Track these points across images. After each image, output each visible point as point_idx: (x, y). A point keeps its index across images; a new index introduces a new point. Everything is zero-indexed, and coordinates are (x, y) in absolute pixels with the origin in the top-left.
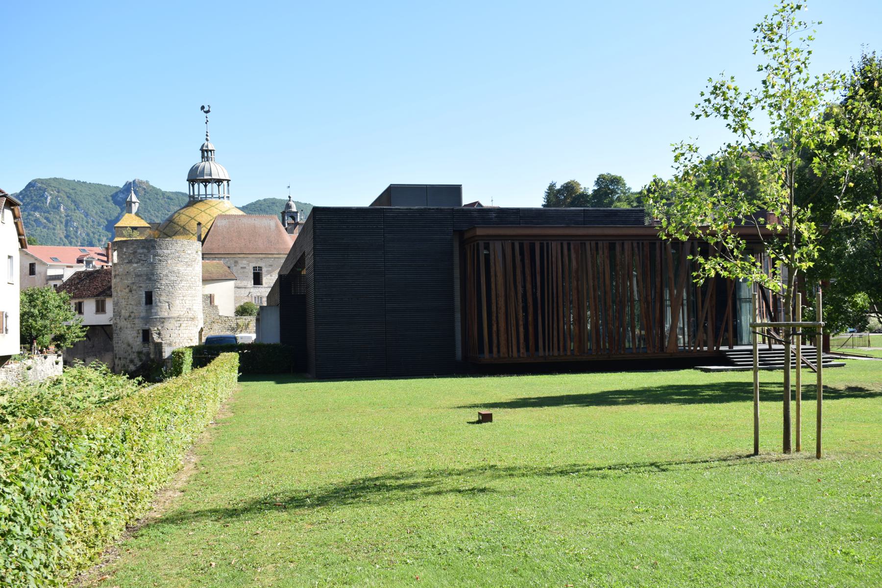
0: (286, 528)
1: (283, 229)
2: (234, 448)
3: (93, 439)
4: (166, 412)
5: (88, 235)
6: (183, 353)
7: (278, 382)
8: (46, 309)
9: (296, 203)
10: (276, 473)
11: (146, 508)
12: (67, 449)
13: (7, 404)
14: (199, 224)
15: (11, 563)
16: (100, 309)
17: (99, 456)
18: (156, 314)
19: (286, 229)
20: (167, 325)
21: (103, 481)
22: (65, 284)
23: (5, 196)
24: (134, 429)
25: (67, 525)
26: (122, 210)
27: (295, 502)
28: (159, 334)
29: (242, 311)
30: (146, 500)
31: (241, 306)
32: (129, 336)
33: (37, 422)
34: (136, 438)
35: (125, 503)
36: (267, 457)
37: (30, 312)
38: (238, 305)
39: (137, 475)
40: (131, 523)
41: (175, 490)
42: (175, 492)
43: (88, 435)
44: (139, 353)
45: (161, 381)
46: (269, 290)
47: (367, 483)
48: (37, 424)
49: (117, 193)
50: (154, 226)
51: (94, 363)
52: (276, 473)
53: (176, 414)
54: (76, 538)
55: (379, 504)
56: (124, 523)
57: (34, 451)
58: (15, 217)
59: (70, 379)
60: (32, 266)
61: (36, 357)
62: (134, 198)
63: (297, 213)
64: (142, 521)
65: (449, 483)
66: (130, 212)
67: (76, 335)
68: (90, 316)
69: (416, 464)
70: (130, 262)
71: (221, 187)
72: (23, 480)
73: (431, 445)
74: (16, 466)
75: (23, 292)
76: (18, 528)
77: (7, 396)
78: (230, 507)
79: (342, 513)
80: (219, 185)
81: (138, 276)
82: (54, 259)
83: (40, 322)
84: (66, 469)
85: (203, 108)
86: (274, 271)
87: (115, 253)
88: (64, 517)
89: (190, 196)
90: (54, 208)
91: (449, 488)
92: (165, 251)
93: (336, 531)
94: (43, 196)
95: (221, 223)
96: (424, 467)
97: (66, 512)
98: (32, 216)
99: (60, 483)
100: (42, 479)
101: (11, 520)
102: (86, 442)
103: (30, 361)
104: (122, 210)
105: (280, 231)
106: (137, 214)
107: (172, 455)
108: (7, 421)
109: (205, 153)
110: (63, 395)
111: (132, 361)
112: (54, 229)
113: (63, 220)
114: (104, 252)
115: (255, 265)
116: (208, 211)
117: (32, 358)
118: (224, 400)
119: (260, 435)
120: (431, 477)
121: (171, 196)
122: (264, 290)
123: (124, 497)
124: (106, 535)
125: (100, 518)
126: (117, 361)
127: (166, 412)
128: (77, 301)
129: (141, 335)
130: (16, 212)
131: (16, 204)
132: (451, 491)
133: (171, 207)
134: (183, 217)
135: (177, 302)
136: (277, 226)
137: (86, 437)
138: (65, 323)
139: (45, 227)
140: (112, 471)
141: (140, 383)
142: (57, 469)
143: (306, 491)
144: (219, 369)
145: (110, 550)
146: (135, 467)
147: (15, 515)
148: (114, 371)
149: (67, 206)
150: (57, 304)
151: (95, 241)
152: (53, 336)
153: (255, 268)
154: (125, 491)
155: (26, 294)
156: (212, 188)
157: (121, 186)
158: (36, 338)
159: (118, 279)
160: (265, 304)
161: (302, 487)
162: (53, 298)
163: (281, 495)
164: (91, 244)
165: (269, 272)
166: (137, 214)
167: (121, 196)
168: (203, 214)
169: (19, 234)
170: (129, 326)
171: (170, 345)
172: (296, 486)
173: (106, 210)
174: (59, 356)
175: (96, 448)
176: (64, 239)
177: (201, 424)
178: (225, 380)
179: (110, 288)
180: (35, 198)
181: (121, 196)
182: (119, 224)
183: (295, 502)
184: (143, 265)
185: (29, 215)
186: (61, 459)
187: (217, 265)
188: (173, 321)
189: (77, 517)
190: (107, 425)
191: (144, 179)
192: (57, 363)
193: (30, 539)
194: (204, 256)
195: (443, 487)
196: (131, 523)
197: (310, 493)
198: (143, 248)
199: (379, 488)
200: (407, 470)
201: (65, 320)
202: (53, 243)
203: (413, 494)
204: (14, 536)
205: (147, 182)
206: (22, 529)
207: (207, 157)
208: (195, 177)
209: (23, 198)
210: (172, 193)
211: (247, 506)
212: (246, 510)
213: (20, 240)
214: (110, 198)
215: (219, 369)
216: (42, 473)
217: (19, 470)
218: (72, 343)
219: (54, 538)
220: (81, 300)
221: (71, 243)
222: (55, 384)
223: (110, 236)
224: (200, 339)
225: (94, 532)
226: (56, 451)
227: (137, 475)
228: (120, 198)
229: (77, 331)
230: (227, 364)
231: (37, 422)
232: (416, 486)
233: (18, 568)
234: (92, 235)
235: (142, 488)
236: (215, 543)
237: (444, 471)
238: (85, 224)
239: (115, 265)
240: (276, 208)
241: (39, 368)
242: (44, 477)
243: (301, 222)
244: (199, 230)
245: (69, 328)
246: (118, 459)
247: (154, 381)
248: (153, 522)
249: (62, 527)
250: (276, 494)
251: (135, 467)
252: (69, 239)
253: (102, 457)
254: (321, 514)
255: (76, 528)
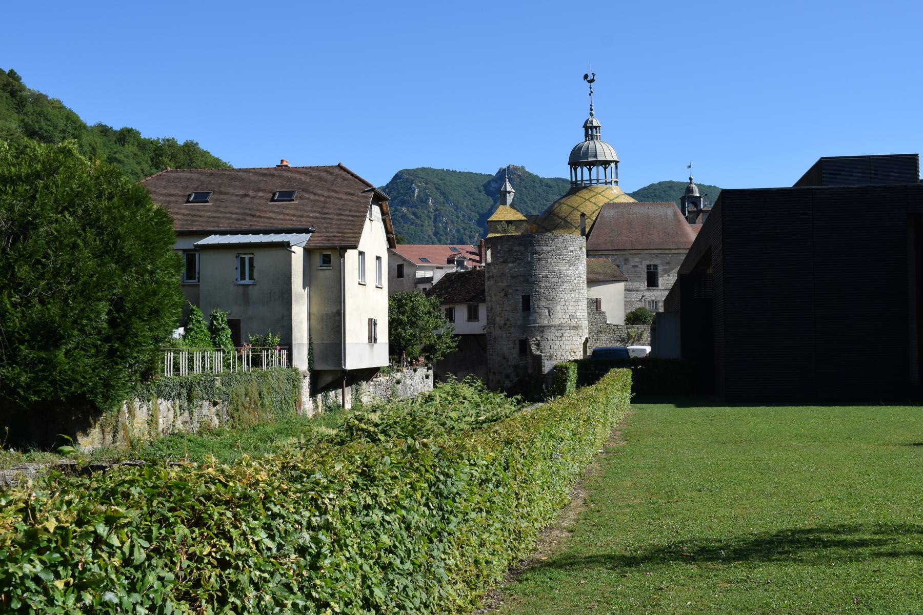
0: (697, 584)
1: (682, 218)
2: (629, 484)
3: (475, 465)
4: (552, 436)
5: (458, 231)
6: (567, 368)
7: (679, 405)
8: (415, 316)
9: (699, 186)
10: (681, 516)
11: (530, 547)
12: (447, 475)
13: (379, 422)
14: (583, 215)
15: (392, 599)
16: (473, 316)
17: (480, 485)
18: (535, 321)
19: (687, 218)
20: (547, 335)
21: (484, 514)
22: (435, 287)
23: (373, 190)
24: (517, 455)
25: (447, 561)
26: (495, 202)
27: (706, 554)
28: (538, 345)
29: (634, 318)
30: (530, 538)
31: (633, 313)
32: (505, 346)
33: (417, 443)
34: (519, 466)
35: (508, 540)
36: (670, 495)
37: (399, 319)
38: (629, 311)
39: (520, 510)
40: (514, 564)
41: (562, 529)
42: (562, 532)
43: (469, 460)
44: (516, 367)
45: (542, 400)
46: (667, 293)
47: (797, 536)
48: (417, 445)
49: (489, 182)
50: (531, 219)
51: (468, 378)
52: (681, 516)
53: (562, 440)
54: (457, 577)
55: (814, 564)
56: (506, 563)
57: (414, 476)
58: (383, 213)
59: (443, 396)
60: (400, 267)
61: (405, 370)
62: (509, 188)
63: (700, 197)
64: (526, 563)
65: (908, 542)
66: (504, 203)
67: (447, 345)
68: (462, 324)
69: (863, 517)
70: (505, 262)
71: (608, 170)
72: (404, 508)
73: (880, 491)
74: (396, 492)
75: (391, 297)
76: (398, 561)
77: (378, 413)
78: (627, 554)
79: (764, 571)
80: (605, 168)
81: (513, 277)
82: (424, 260)
83: (410, 331)
84: (447, 498)
85: (586, 77)
86: (673, 269)
87: (489, 252)
88: (444, 553)
89: (572, 182)
90: (422, 201)
91: (908, 549)
92: (545, 248)
93: (760, 593)
94: (410, 189)
95: (609, 213)
96: (872, 520)
97: (447, 547)
98: (399, 211)
99: (441, 513)
100: (423, 508)
101: (391, 552)
102: (467, 469)
103: (399, 374)
104: (495, 202)
105: (679, 221)
106: (512, 206)
107: (558, 488)
108: (379, 440)
109: (590, 130)
110: (436, 414)
111: (507, 376)
112: (422, 226)
113: (432, 216)
114: (477, 251)
115: (648, 262)
116: (593, 200)
117: (402, 371)
118: (615, 426)
119: (659, 469)
120: (883, 533)
121: (550, 183)
122: (660, 294)
123: (506, 534)
124: (488, 576)
125: (481, 556)
126: (491, 376)
127: (552, 436)
128: (448, 307)
129: (518, 346)
130: (385, 208)
131: (385, 199)
132: (912, 553)
133: (550, 196)
134: (564, 207)
135: (559, 307)
136: (675, 215)
137: (467, 462)
138: (435, 332)
139: (412, 224)
140: (494, 503)
141: (519, 402)
142: (437, 498)
143: (720, 541)
144: (610, 388)
145: (492, 594)
146: (518, 499)
147: (395, 546)
148: (493, 389)
149: (435, 199)
150: (426, 310)
151: (466, 238)
152: (423, 345)
153: (649, 267)
154: (507, 525)
155: (394, 299)
156: (598, 172)
157: (494, 174)
158: (405, 348)
159: (492, 282)
160: (661, 310)
161: (714, 535)
162: (423, 304)
163: (689, 544)
164: (462, 242)
165: (666, 272)
166: (512, 206)
167: (494, 185)
168: (587, 203)
169: (388, 232)
170: (504, 335)
171: (550, 358)
172: (707, 534)
173: (478, 202)
174: (429, 369)
175: (478, 476)
176: (433, 237)
177: (590, 452)
178: (616, 401)
179: (484, 291)
180: (401, 191)
181: (494, 185)
182: (494, 218)
183: (706, 554)
184: (519, 264)
185: (396, 210)
186: (442, 486)
187: (604, 263)
188: (553, 330)
189: (457, 553)
190: (489, 450)
191: (519, 165)
192: (427, 377)
193: (410, 574)
194: (589, 253)
195: (899, 547)
196: (514, 564)
197: (724, 543)
198: (520, 245)
199: (813, 544)
200: (849, 522)
201: (436, 328)
202: (421, 242)
203: (860, 553)
204: (394, 570)
205: (523, 168)
206: (402, 563)
207: (592, 135)
208: (578, 159)
209: (390, 191)
210: (551, 179)
211: (647, 553)
212: (645, 559)
213: (389, 239)
214: (482, 188)
215: (610, 388)
216: (423, 501)
217: (400, 496)
218: (443, 354)
219: (434, 576)
220: (452, 306)
221: (440, 241)
222: (426, 401)
223: (482, 232)
224: (585, 351)
225: (475, 571)
226: (437, 477)
227: (520, 510)
228: (493, 187)
229: (448, 341)
230: (618, 382)
231: (417, 443)
232: (862, 543)
233: (398, 606)
234: (462, 231)
235: (526, 524)
236: (612, 596)
237: (901, 526)
238: (455, 219)
239: (488, 265)
240: (674, 193)
241: (408, 382)
242: (424, 506)
243: (706, 209)
244: (583, 222)
245: (440, 337)
246: (501, 489)
247: (534, 400)
248: (539, 565)
249: (442, 564)
250: (682, 542)
251: (518, 499)
252: (438, 237)
253: (484, 486)
254: (739, 571)
255: (456, 565)
